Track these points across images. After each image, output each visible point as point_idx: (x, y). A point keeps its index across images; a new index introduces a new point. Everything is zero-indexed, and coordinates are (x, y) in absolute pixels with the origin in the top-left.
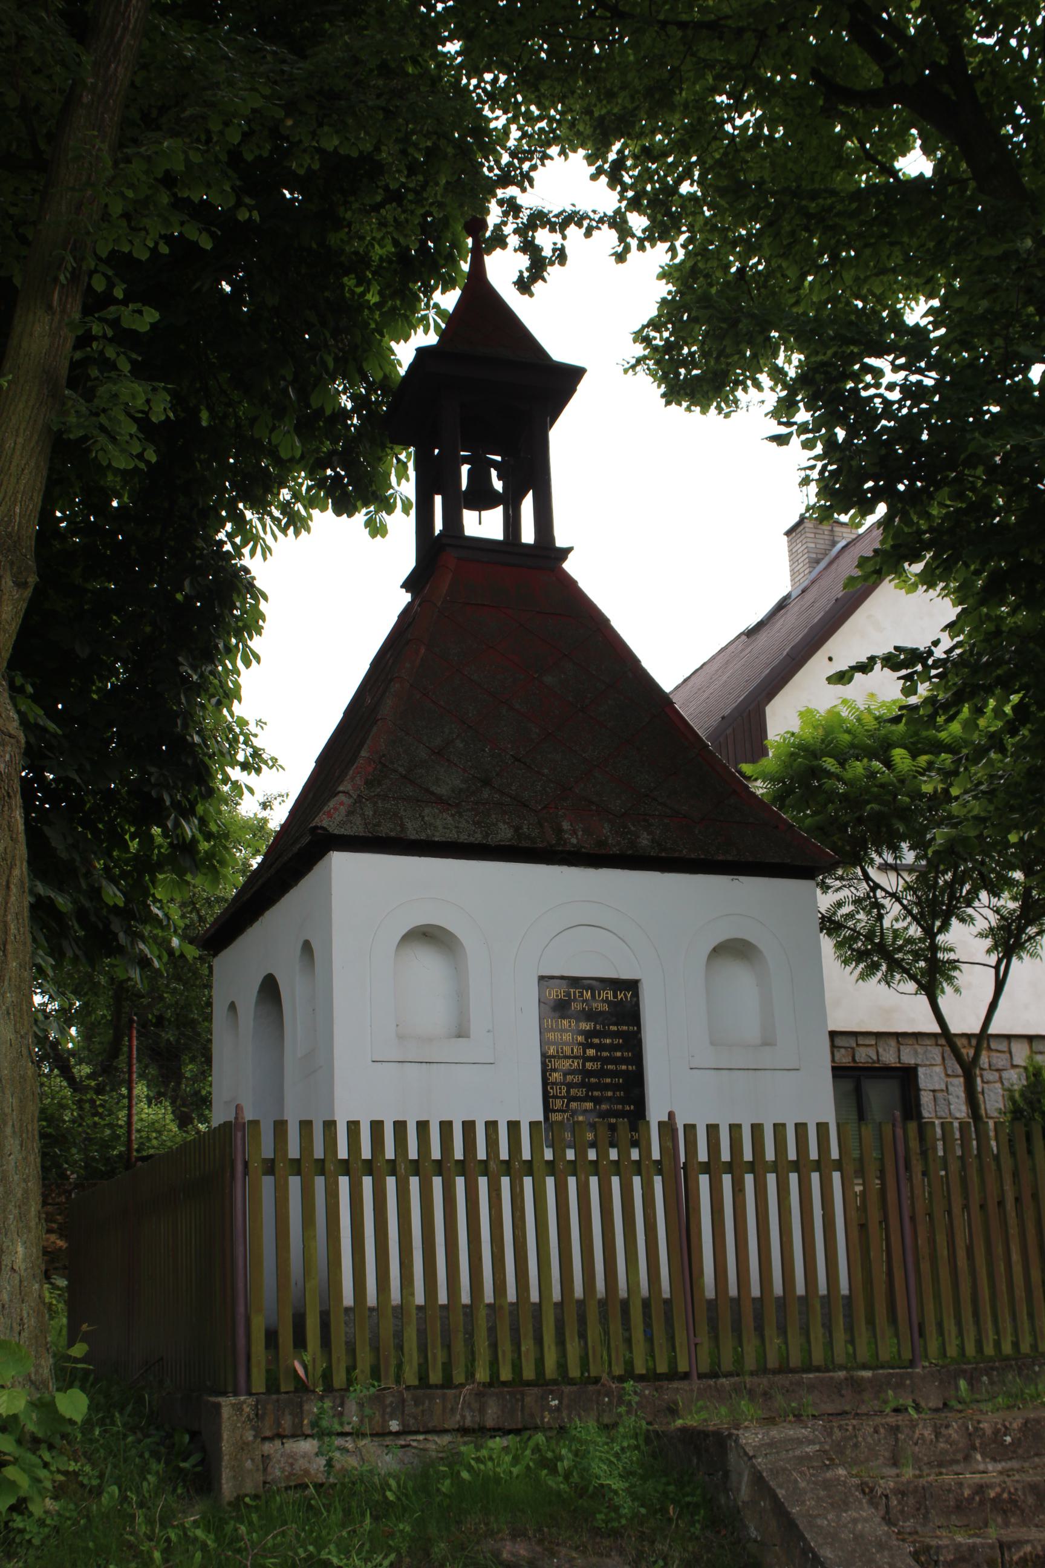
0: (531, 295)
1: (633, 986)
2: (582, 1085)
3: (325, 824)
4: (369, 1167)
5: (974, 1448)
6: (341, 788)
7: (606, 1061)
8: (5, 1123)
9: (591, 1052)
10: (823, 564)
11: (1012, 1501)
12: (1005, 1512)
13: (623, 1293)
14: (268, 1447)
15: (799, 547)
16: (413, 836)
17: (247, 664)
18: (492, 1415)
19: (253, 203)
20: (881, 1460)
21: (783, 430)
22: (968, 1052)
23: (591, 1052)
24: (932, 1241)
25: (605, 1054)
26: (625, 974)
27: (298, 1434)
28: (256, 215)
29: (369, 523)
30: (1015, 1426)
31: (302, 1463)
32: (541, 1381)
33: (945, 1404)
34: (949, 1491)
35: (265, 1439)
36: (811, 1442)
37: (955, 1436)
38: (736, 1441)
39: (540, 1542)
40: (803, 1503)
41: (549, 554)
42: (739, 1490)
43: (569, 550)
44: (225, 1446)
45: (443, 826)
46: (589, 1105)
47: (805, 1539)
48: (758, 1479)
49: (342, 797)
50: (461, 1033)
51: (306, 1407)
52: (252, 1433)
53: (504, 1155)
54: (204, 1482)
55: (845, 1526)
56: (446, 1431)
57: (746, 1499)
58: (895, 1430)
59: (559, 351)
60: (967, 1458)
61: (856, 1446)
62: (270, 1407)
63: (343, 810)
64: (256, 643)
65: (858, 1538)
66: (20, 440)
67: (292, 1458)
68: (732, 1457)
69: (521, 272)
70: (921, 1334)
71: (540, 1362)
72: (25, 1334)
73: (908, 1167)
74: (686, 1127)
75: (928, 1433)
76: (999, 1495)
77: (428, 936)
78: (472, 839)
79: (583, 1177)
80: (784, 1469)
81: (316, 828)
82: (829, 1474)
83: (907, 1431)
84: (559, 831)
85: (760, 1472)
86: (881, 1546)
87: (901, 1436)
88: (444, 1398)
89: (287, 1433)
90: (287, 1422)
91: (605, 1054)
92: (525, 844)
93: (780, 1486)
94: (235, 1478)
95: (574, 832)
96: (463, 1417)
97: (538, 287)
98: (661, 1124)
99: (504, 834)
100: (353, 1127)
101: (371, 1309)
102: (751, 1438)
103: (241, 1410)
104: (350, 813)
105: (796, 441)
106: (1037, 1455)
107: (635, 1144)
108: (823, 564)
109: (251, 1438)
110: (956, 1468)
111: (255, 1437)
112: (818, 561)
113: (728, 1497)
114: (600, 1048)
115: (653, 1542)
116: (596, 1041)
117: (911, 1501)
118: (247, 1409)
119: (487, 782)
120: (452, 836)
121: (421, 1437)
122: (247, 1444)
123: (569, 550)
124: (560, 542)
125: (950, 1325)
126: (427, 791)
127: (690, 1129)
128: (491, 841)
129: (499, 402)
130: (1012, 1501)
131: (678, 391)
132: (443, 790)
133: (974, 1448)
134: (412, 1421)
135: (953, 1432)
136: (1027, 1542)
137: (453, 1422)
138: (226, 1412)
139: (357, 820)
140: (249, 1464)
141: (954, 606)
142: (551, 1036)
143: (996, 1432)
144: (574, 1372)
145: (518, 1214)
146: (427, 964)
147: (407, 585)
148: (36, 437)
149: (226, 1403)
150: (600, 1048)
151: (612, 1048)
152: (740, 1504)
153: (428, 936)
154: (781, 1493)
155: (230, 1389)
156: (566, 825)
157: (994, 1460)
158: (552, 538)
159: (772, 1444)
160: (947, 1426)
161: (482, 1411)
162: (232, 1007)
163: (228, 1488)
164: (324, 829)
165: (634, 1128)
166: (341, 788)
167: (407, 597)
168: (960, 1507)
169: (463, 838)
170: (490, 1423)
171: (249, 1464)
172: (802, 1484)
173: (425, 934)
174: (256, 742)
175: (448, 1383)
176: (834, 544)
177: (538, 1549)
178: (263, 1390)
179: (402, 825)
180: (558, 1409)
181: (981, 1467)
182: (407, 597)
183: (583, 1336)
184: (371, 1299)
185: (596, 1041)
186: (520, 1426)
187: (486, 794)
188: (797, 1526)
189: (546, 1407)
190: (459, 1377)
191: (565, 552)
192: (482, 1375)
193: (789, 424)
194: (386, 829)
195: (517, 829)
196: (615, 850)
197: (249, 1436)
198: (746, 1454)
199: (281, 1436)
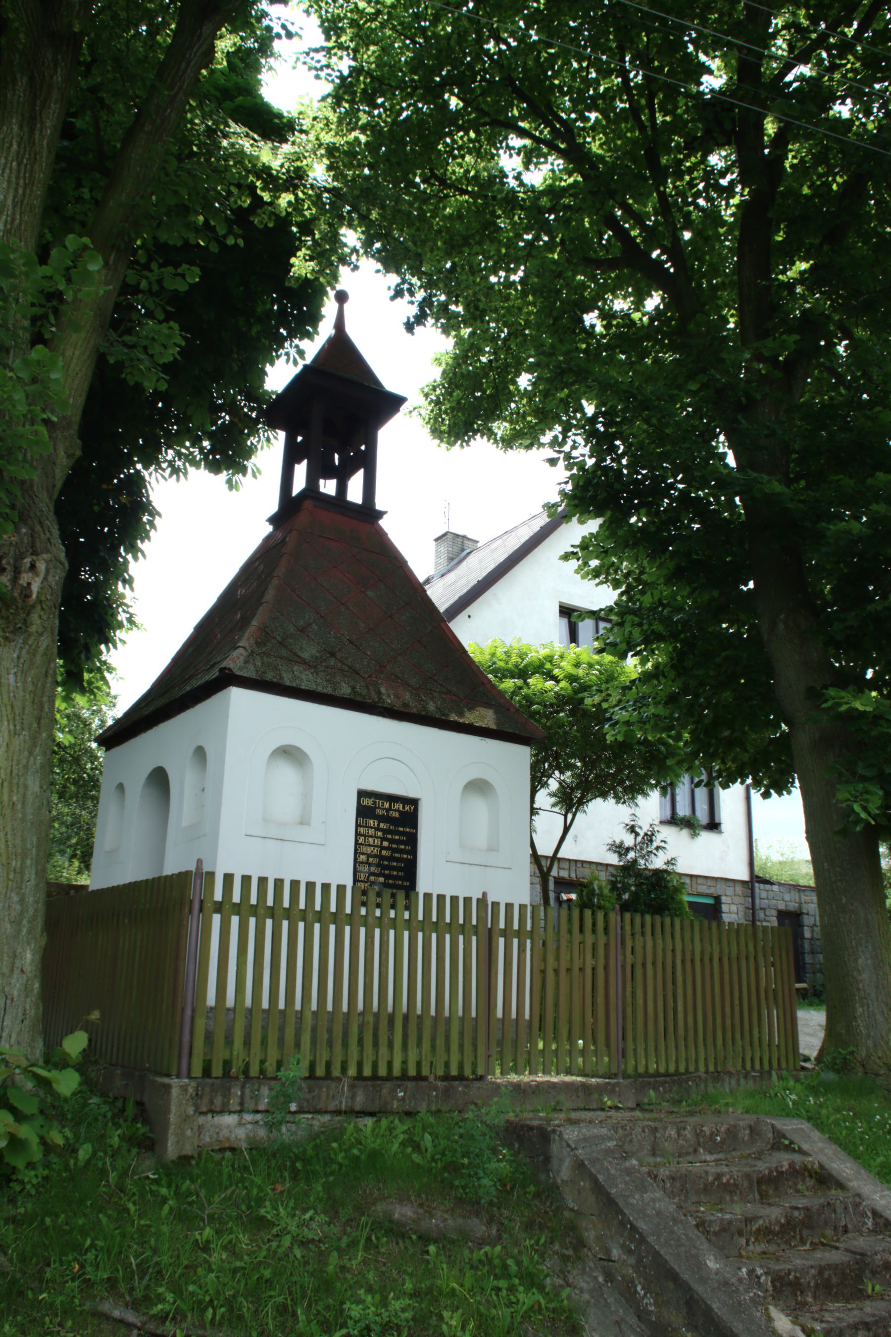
0: (413, 334)
1: (414, 802)
2: (378, 865)
3: (231, 666)
4: (288, 914)
5: (699, 1145)
6: (240, 644)
7: (394, 851)
8: (645, 891)
9: (386, 844)
10: (455, 561)
11: (735, 1185)
12: (731, 1192)
13: (390, 1009)
14: (201, 1120)
15: (443, 549)
16: (288, 683)
17: (136, 558)
18: (360, 1101)
19: (241, 232)
20: (645, 1151)
21: (556, 455)
22: (545, 864)
23: (386, 844)
24: (633, 993)
25: (394, 846)
26: (412, 795)
27: (224, 1110)
28: (241, 242)
29: (229, 482)
30: (723, 1129)
31: (225, 1133)
32: (389, 1078)
33: (638, 1105)
34: (701, 1177)
35: (201, 1113)
36: (610, 1139)
37: (689, 1136)
38: (560, 1136)
39: (421, 1205)
40: (616, 1186)
41: (368, 513)
42: (559, 1172)
43: (384, 513)
44: (173, 1118)
45: (307, 680)
46: (381, 879)
47: (623, 1214)
48: (580, 1166)
49: (241, 650)
50: (302, 823)
51: (233, 1091)
52: (193, 1108)
53: (270, 902)
54: (150, 1144)
55: (648, 1204)
56: (326, 1112)
57: (565, 1178)
58: (655, 1130)
59: (390, 383)
60: (695, 1151)
61: (631, 1141)
62: (207, 1089)
63: (242, 659)
64: (142, 545)
65: (659, 1213)
66: (77, 353)
67: (219, 1127)
68: (555, 1148)
69: (408, 318)
70: (623, 1056)
71: (390, 1064)
72: (26, 1022)
73: (623, 943)
74: (493, 903)
75: (673, 1133)
76: (728, 1181)
77: (289, 753)
78: (325, 691)
79: (427, 933)
80: (598, 1159)
81: (225, 668)
82: (627, 1164)
83: (661, 1131)
84: (379, 693)
85: (582, 1161)
86: (675, 1221)
87: (658, 1135)
88: (328, 1088)
89: (218, 1109)
90: (218, 1102)
91: (394, 846)
92: (359, 698)
93: (599, 1172)
94: (178, 1142)
95: (389, 696)
96: (341, 1103)
97: (418, 329)
98: (478, 900)
99: (345, 690)
100: (228, 878)
101: (229, 1010)
102: (571, 1134)
103: (186, 1090)
104: (246, 662)
105: (561, 464)
106: (734, 1150)
107: (407, 908)
108: (455, 561)
109: (192, 1113)
110: (690, 1158)
111: (195, 1111)
112: (452, 559)
113: (548, 1176)
114: (391, 841)
115: (499, 1208)
116: (389, 836)
117: (678, 1184)
118: (190, 1090)
119: (333, 654)
120: (313, 687)
121: (310, 1116)
122: (188, 1117)
123: (384, 513)
124: (379, 506)
125: (641, 1052)
126: (295, 654)
127: (496, 905)
128: (339, 693)
129: (340, 412)
130: (735, 1185)
131: (436, 432)
132: (306, 655)
133: (699, 1145)
134: (305, 1104)
135: (688, 1133)
136: (761, 1217)
137: (332, 1107)
138: (175, 1092)
139: (252, 667)
140: (189, 1133)
141: (614, 589)
142: (361, 830)
143: (712, 1133)
144: (412, 1072)
145: (384, 956)
146: (286, 773)
147: (273, 520)
148: (88, 353)
149: (175, 1082)
150: (391, 841)
151: (398, 842)
152: (559, 1181)
153: (289, 753)
154: (601, 1177)
155: (174, 1072)
156: (383, 690)
157: (711, 1153)
158: (373, 504)
159: (585, 1139)
160: (685, 1129)
161: (353, 1098)
162: (121, 787)
163: (172, 1150)
164: (229, 669)
165: (407, 897)
166: (240, 644)
167: (269, 528)
168: (707, 1189)
169: (320, 689)
170: (358, 1108)
171: (189, 1133)
172: (613, 1171)
173: (285, 752)
174: (130, 610)
175: (328, 1076)
176: (463, 550)
177: (421, 1211)
178: (200, 1075)
179: (280, 675)
180: (403, 1099)
181: (703, 1158)
182: (269, 528)
183: (419, 1044)
184: (230, 1001)
185: (389, 836)
186: (377, 1110)
187: (332, 662)
188: (617, 1205)
189: (395, 1097)
190: (336, 1072)
191: (380, 514)
192: (352, 1072)
193: (559, 452)
194: (270, 676)
195: (353, 688)
196: (414, 711)
197: (191, 1110)
198: (568, 1145)
199: (213, 1112)
